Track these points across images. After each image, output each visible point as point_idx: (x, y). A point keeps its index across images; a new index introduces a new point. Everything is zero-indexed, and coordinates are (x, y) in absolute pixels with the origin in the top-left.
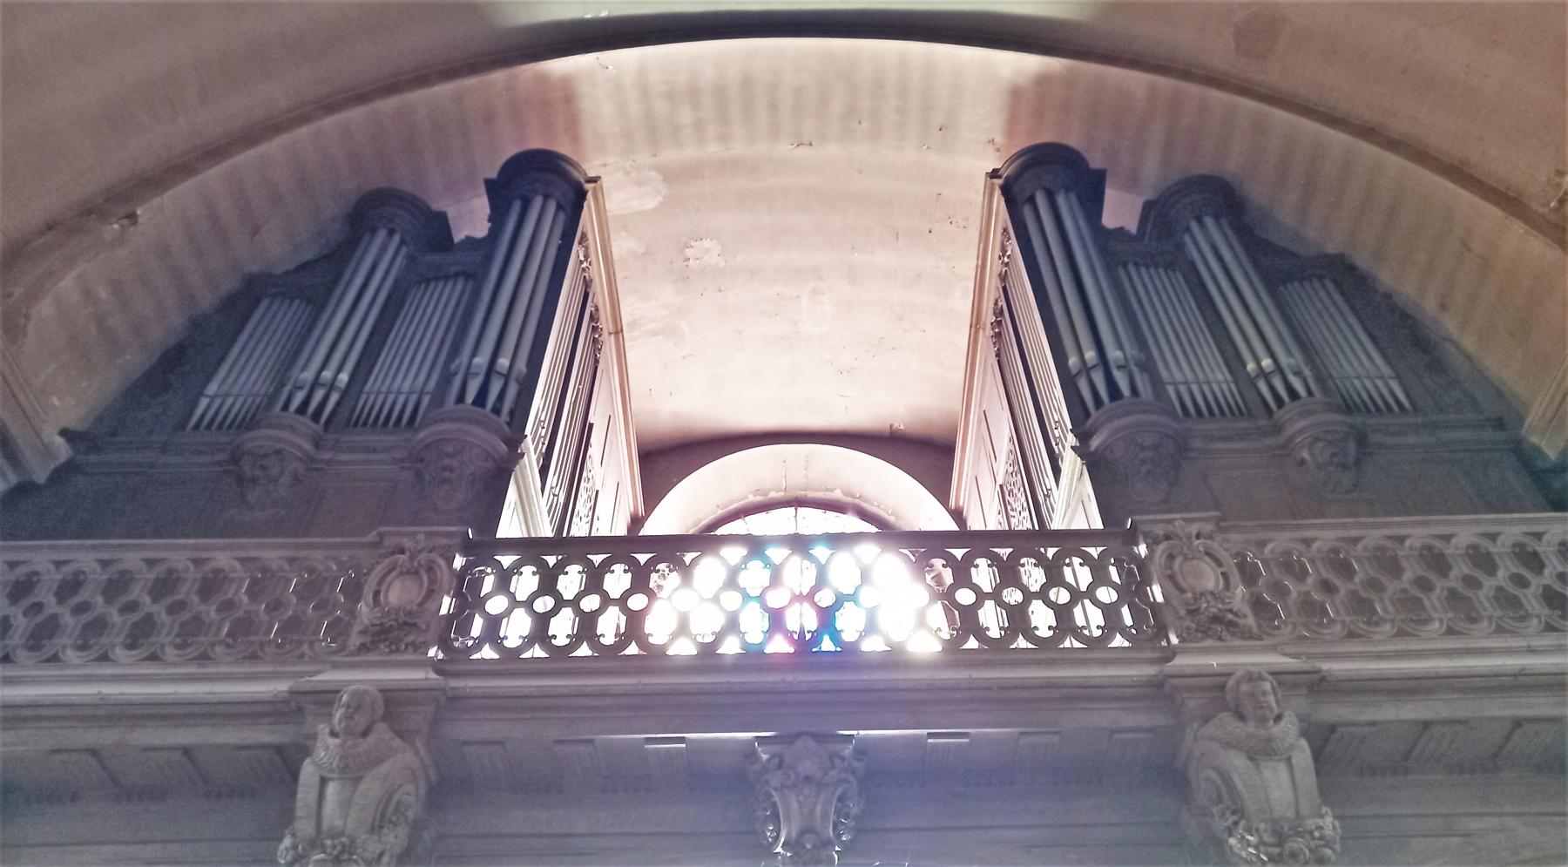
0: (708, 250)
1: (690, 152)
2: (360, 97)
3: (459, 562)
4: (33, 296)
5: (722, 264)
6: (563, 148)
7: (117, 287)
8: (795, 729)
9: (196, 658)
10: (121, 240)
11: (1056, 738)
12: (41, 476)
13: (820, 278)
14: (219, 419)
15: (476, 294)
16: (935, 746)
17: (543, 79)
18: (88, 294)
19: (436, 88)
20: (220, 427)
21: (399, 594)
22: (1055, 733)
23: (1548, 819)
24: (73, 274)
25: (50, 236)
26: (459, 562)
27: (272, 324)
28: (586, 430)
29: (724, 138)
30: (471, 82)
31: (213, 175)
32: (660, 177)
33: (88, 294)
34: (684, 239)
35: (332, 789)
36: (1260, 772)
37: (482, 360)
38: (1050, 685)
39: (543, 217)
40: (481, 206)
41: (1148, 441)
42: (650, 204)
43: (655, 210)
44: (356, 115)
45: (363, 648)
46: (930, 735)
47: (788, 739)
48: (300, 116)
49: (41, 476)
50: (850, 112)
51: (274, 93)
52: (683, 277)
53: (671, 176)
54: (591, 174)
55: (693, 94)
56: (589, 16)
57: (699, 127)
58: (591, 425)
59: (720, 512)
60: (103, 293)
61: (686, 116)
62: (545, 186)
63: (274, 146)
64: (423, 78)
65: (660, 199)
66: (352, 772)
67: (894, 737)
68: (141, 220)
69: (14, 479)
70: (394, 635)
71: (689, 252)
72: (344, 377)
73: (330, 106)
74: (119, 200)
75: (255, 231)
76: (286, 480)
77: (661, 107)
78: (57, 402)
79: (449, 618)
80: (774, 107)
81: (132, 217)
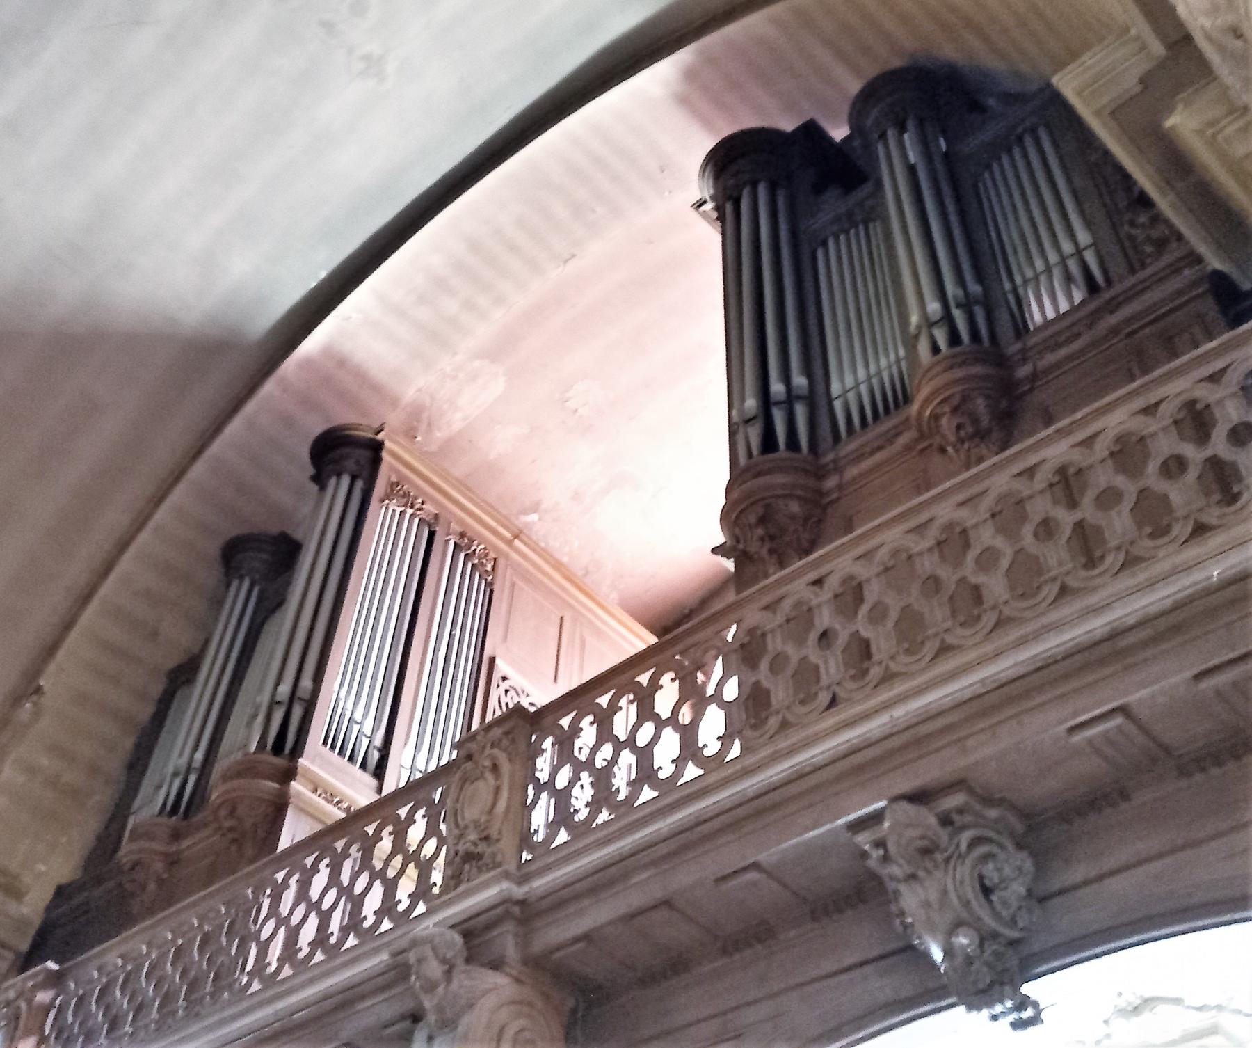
2: (178, 475)
7: (56, 750)
9: (1123, 566)
10: (37, 714)
11: (1118, 720)
14: (890, 399)
17: (308, 363)
18: (31, 770)
20: (864, 422)
22: (1113, 712)
23: (824, 983)
29: (499, 300)
30: (250, 407)
33: (31, 770)
41: (752, 519)
42: (498, 387)
48: (140, 523)
51: (115, 517)
53: (495, 352)
54: (376, 425)
55: (441, 284)
56: (313, 284)
57: (469, 305)
58: (492, 660)
60: (45, 762)
61: (451, 306)
62: (347, 455)
63: (126, 563)
68: (46, 689)
69: (10, 956)
72: (199, 756)
73: (158, 500)
75: (154, 634)
76: (152, 886)
78: (43, 868)
80: (513, 248)
81: (38, 690)
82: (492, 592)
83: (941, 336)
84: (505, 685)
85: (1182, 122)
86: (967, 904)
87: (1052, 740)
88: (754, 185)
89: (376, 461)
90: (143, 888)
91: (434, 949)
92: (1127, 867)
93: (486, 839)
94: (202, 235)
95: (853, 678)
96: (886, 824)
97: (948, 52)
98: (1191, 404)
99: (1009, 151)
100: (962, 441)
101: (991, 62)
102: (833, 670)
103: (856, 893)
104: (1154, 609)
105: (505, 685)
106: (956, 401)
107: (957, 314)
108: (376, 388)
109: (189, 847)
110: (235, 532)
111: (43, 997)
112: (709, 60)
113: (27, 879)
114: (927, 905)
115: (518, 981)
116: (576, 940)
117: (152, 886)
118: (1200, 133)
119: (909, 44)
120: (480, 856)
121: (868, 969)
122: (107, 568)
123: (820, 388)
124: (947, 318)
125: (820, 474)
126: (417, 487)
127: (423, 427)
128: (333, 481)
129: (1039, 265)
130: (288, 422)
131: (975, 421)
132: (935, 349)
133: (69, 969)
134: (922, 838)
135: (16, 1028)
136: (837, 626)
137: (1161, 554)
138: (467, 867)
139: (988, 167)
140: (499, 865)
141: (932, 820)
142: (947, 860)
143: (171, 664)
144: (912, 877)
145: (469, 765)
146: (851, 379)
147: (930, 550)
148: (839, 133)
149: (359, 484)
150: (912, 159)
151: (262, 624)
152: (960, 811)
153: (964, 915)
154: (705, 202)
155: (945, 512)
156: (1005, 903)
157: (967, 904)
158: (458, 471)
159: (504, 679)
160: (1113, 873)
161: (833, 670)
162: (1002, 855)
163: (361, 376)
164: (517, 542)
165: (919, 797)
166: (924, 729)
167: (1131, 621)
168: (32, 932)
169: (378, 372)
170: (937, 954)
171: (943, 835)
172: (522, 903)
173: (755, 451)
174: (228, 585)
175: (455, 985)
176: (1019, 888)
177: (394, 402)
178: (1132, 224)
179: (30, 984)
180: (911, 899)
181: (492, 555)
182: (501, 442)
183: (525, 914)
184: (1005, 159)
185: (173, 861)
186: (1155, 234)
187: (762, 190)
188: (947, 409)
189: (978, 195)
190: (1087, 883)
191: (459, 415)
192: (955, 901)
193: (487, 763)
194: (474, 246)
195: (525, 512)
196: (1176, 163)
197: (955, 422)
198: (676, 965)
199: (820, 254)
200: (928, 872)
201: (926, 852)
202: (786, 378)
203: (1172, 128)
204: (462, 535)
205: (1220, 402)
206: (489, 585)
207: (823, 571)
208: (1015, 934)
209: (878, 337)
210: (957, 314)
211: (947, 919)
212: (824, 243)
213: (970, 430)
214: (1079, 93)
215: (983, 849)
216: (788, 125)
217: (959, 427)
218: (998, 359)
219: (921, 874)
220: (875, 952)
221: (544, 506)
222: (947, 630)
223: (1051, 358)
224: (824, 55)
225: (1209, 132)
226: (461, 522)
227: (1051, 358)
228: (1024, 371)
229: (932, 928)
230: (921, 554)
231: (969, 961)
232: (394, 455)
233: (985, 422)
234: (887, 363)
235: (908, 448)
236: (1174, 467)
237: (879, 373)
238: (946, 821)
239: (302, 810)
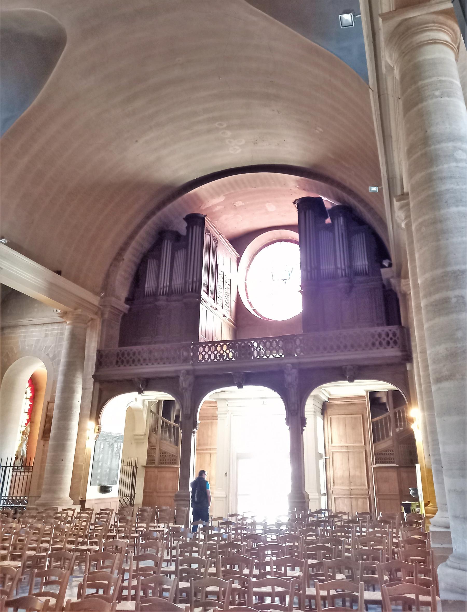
3: (192, 347)
15: (187, 253)
17: (190, 195)
21: (185, 354)
26: (192, 347)
27: (152, 265)
28: (217, 265)
35: (183, 383)
37: (191, 280)
39: (197, 230)
40: (185, 224)
42: (222, 200)
49: (127, 312)
66: (185, 380)
69: (123, 313)
70: (186, 360)
72: (168, 283)
83: (343, 273)
124: (345, 270)
180: (347, 373)
236: (384, 339)
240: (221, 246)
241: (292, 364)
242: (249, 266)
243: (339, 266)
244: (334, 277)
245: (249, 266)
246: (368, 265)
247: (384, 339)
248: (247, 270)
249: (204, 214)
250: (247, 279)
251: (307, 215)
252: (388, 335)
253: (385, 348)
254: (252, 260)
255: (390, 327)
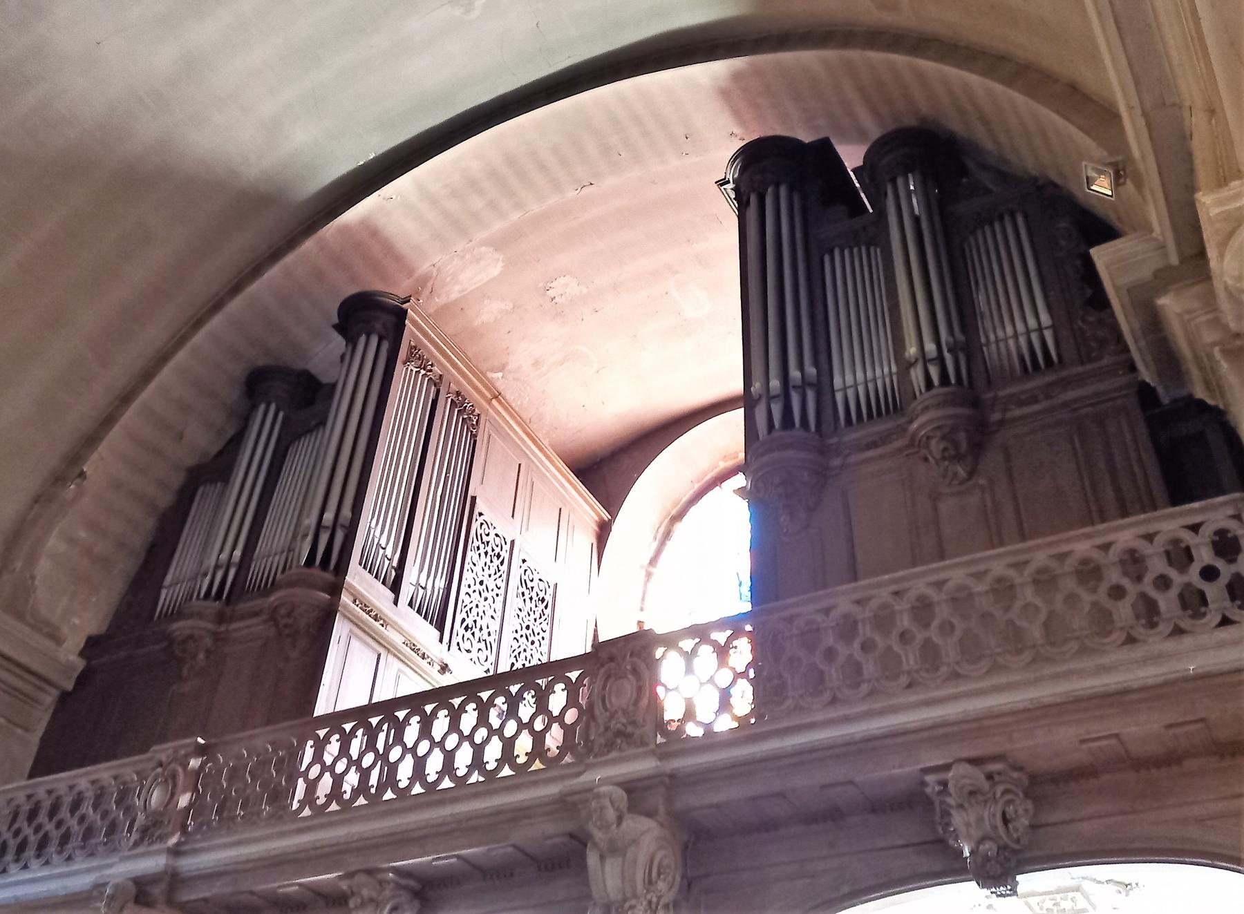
0: (567, 285)
1: (498, 226)
2: (216, 306)
4: (31, 561)
5: (585, 291)
6: (377, 286)
8: (353, 868)
12: (69, 686)
13: (677, 272)
16: (436, 867)
17: (345, 229)
18: (71, 541)
19: (266, 276)
24: (55, 532)
25: (37, 507)
28: (468, 505)
29: (519, 205)
30: (290, 259)
31: (130, 416)
32: (491, 249)
34: (541, 285)
36: (603, 866)
38: (498, 812)
41: (777, 481)
42: (495, 271)
43: (502, 273)
44: (216, 323)
45: (136, 844)
46: (434, 860)
47: (350, 875)
48: (179, 341)
49: (69, 686)
50: (606, 150)
51: (154, 334)
52: (558, 312)
53: (498, 244)
55: (473, 184)
57: (492, 205)
58: (474, 499)
59: (697, 486)
60: (83, 534)
61: (477, 203)
62: (374, 319)
63: (166, 374)
64: (256, 270)
65: (500, 264)
67: (421, 863)
69: (55, 693)
71: (551, 293)
72: (238, 553)
74: (70, 468)
75: (180, 436)
76: (201, 656)
77: (452, 205)
79: (187, 809)
80: (542, 167)
81: (82, 475)
82: (475, 442)
83: (934, 372)
84: (481, 520)
85: (1170, 304)
86: (995, 828)
87: (1064, 742)
88: (777, 186)
89: (399, 328)
90: (194, 657)
91: (612, 803)
92: (1090, 818)
93: (634, 723)
94: (282, 110)
95: (927, 671)
96: (951, 774)
97: (955, 125)
98: (1176, 542)
99: (991, 224)
100: (944, 458)
101: (989, 145)
102: (912, 662)
103: (914, 803)
104: (1151, 681)
105: (481, 520)
106: (947, 430)
107: (947, 356)
108: (398, 258)
109: (236, 630)
110: (261, 362)
111: (194, 763)
112: (757, 72)
113: (65, 630)
114: (968, 825)
115: (662, 825)
116: (710, 806)
117: (201, 656)
118: (1180, 315)
119: (925, 108)
120: (630, 735)
121: (910, 849)
122: (146, 376)
123: (826, 379)
124: (940, 360)
125: (823, 451)
126: (429, 351)
127: (427, 292)
128: (363, 339)
129: (1009, 330)
130: (319, 275)
131: (956, 446)
132: (929, 384)
133: (215, 745)
134: (972, 785)
135: (175, 786)
136: (914, 630)
137: (1151, 640)
138: (619, 741)
139: (973, 233)
140: (647, 744)
141: (982, 777)
142: (986, 802)
143: (191, 461)
144: (961, 806)
145: (613, 664)
146: (854, 378)
147: (987, 592)
148: (852, 156)
149: (385, 346)
150: (917, 211)
151: (287, 449)
152: (999, 773)
153: (992, 834)
154: (728, 182)
155: (998, 569)
156: (1017, 830)
157: (995, 828)
158: (450, 329)
159: (481, 514)
160: (1082, 820)
161: (912, 662)
162: (1018, 802)
163: (388, 248)
164: (494, 401)
165: (975, 761)
166: (987, 723)
167: (1135, 685)
168: (76, 675)
169: (402, 246)
170: (967, 853)
171: (986, 785)
172: (672, 776)
173: (777, 424)
174: (254, 407)
175: (624, 826)
176: (1025, 821)
177: (410, 271)
178: (1084, 320)
179: (183, 752)
180: (958, 819)
181: (477, 411)
182: (488, 312)
183: (674, 782)
184: (987, 228)
185: (218, 638)
186: (1100, 333)
187: (783, 191)
188: (939, 434)
189: (964, 256)
190: (1063, 823)
191: (457, 288)
192: (987, 823)
193: (629, 667)
194: (511, 161)
195: (494, 370)
196: (1154, 324)
197: (942, 446)
198: (768, 826)
199: (827, 258)
200: (971, 804)
201: (972, 793)
202: (801, 366)
203: (1163, 306)
204: (458, 394)
205: (1197, 545)
206: (474, 436)
207: (906, 585)
208: (1016, 847)
209: (875, 352)
210: (947, 356)
211: (976, 833)
212: (831, 252)
213: (953, 453)
214: (1107, 267)
215: (1008, 797)
216: (806, 137)
217: (945, 450)
218: (975, 403)
219: (966, 805)
220: (915, 840)
221: (509, 367)
222: (999, 654)
223: (1018, 412)
224: (851, 94)
225: (1187, 317)
226: (458, 383)
227: (1018, 412)
228: (996, 416)
229: (969, 837)
230: (979, 594)
231: (987, 859)
232: (415, 323)
233: (964, 446)
234: (884, 372)
235: (900, 450)
236: (1163, 583)
237: (875, 380)
238: (990, 777)
239: (345, 617)
240: (498, 444)
241: (632, 788)
242: (653, 561)
243: (912, 350)
244: (888, 406)
245: (653, 561)
246: (1053, 327)
247: (1163, 583)
248: (649, 575)
249: (401, 292)
250: (646, 606)
251: (769, 201)
252: (1181, 556)
253: (1178, 631)
254: (667, 535)
255: (1194, 510)
